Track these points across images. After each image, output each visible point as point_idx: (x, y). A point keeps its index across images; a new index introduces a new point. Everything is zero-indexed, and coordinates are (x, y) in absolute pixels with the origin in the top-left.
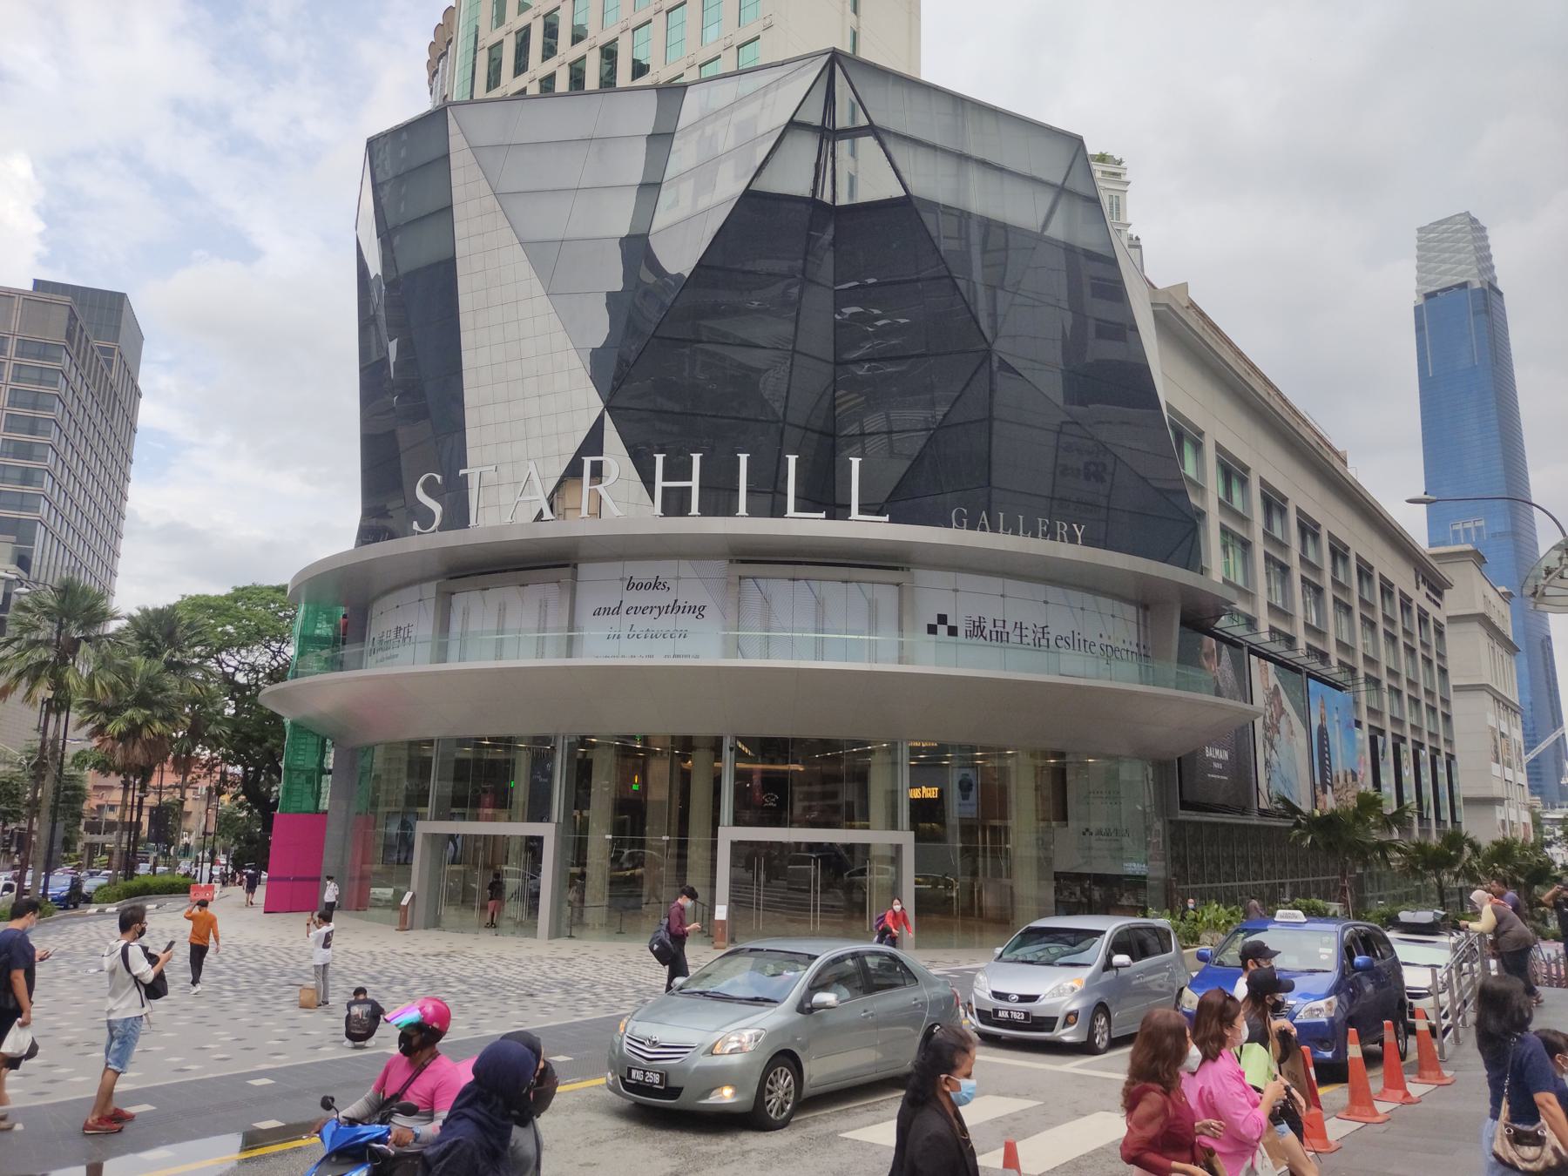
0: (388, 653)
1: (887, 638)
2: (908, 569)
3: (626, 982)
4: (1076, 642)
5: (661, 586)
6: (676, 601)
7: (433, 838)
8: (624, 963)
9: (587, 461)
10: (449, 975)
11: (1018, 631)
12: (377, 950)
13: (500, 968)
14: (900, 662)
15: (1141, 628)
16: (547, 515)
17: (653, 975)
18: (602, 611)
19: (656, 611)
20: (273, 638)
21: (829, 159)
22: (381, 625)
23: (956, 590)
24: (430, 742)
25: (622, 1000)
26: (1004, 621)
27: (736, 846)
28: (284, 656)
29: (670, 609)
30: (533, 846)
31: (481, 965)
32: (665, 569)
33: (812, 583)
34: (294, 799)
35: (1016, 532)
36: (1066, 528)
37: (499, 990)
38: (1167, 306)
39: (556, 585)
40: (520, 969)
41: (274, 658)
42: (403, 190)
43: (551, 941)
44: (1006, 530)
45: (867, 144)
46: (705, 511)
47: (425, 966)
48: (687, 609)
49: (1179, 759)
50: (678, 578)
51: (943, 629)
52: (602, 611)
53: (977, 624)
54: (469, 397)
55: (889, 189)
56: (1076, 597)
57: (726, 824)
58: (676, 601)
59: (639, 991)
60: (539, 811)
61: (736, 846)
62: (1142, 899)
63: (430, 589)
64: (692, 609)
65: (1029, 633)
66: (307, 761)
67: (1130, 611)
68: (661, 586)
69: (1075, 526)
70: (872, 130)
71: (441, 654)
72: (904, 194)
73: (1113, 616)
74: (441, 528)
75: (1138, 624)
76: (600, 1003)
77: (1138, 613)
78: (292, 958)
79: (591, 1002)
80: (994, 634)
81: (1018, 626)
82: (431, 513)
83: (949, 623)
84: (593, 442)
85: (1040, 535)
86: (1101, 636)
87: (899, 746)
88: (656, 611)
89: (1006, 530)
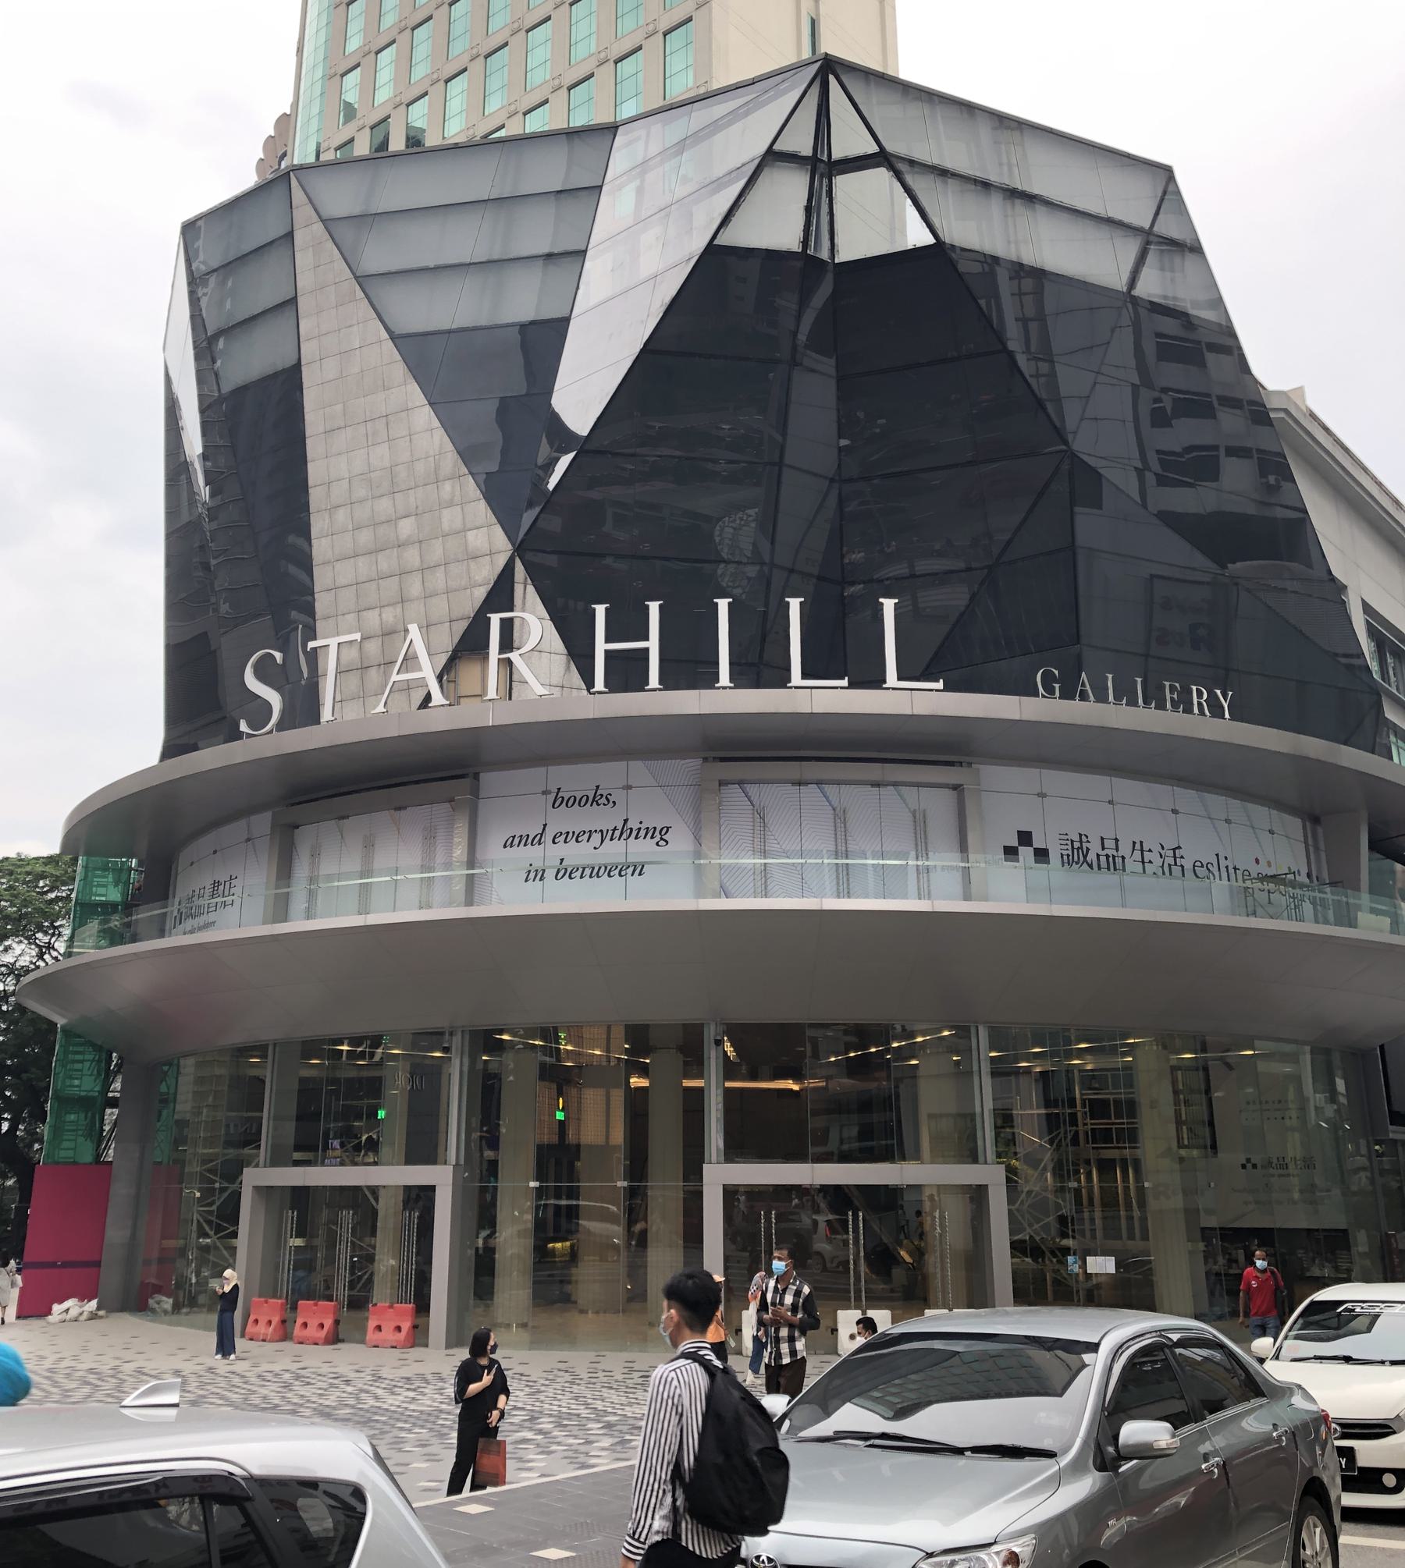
0: (201, 920)
1: (943, 861)
2: (970, 764)
3: (584, 1412)
4: (1223, 869)
5: (604, 800)
6: (626, 821)
7: (265, 1192)
8: (572, 1383)
9: (495, 619)
10: (301, 1405)
11: (1137, 854)
12: (188, 1368)
13: (379, 1392)
14: (967, 897)
15: (1311, 849)
16: (438, 698)
17: (624, 1400)
18: (516, 841)
19: (596, 837)
20: (40, 928)
21: (825, 200)
22: (190, 882)
23: (1042, 795)
24: (261, 1049)
25: (588, 1442)
26: (1117, 840)
27: (730, 1193)
28: (55, 954)
29: (617, 833)
30: (421, 1198)
31: (349, 1389)
32: (607, 774)
33: (827, 788)
34: (65, 1144)
35: (1133, 702)
36: (1205, 696)
37: (387, 1428)
38: (1286, 411)
39: (447, 805)
40: (411, 1394)
41: (41, 956)
42: (230, 284)
43: (451, 1351)
44: (1118, 698)
45: (881, 176)
46: (669, 681)
47: (264, 1391)
48: (642, 833)
49: (1382, 1047)
50: (629, 787)
51: (1026, 853)
52: (516, 841)
53: (1076, 845)
54: (321, 548)
55: (917, 236)
56: (1218, 803)
57: (714, 1158)
58: (626, 821)
59: (609, 1426)
60: (423, 1150)
61: (730, 1193)
62: (1345, 1266)
63: (262, 822)
64: (651, 832)
65: (1153, 856)
66: (86, 1084)
67: (1295, 824)
68: (604, 800)
69: (1218, 692)
70: (882, 158)
71: (280, 910)
72: (931, 240)
73: (1271, 832)
74: (281, 726)
75: (1306, 842)
76: (554, 1447)
77: (1304, 828)
78: (55, 1384)
79: (538, 1445)
80: (1103, 859)
81: (1138, 846)
82: (267, 707)
83: (1032, 849)
84: (501, 595)
85: (1168, 705)
86: (1257, 861)
87: (973, 1031)
88: (596, 837)
89: (1118, 698)
